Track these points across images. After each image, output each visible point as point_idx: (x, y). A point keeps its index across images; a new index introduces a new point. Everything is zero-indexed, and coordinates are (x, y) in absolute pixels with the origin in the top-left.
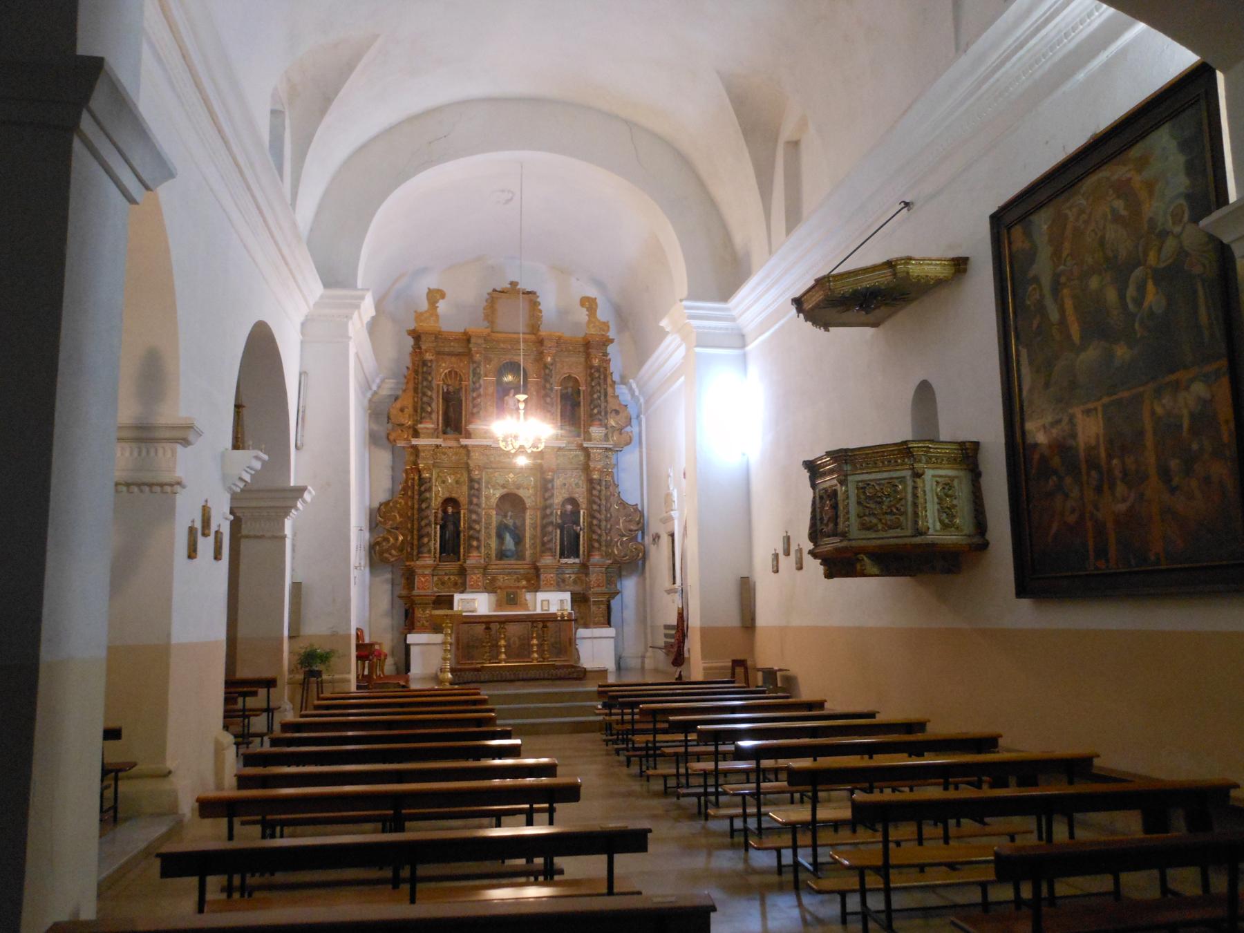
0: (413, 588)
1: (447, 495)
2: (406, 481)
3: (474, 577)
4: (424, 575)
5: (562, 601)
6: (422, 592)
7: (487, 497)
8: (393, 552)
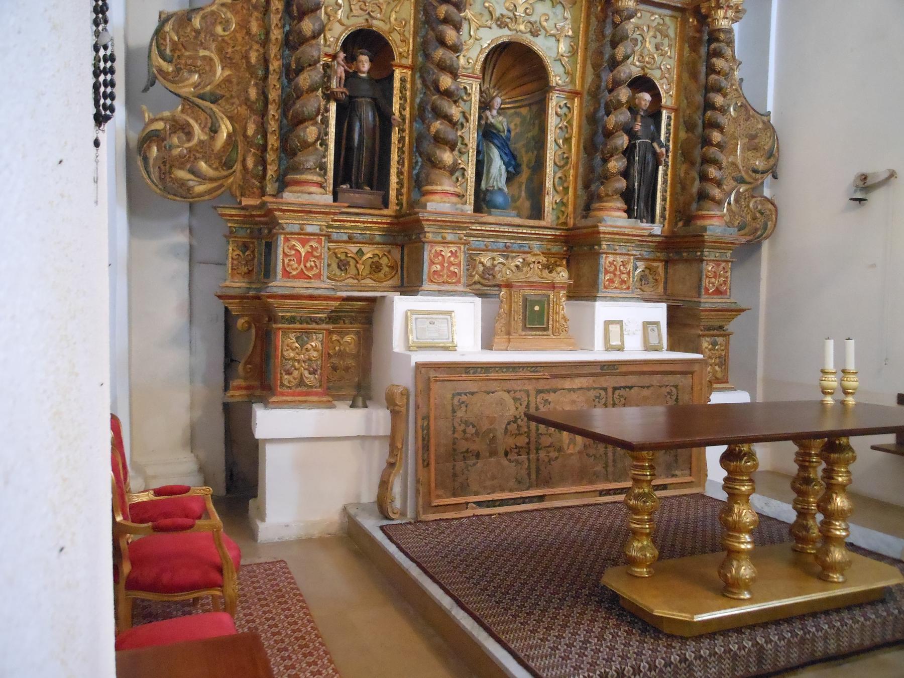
0: (268, 271)
1: (358, 22)
3: (440, 253)
4: (304, 237)
5: (646, 325)
6: (299, 286)
7: (311, 134)
8: (203, 165)
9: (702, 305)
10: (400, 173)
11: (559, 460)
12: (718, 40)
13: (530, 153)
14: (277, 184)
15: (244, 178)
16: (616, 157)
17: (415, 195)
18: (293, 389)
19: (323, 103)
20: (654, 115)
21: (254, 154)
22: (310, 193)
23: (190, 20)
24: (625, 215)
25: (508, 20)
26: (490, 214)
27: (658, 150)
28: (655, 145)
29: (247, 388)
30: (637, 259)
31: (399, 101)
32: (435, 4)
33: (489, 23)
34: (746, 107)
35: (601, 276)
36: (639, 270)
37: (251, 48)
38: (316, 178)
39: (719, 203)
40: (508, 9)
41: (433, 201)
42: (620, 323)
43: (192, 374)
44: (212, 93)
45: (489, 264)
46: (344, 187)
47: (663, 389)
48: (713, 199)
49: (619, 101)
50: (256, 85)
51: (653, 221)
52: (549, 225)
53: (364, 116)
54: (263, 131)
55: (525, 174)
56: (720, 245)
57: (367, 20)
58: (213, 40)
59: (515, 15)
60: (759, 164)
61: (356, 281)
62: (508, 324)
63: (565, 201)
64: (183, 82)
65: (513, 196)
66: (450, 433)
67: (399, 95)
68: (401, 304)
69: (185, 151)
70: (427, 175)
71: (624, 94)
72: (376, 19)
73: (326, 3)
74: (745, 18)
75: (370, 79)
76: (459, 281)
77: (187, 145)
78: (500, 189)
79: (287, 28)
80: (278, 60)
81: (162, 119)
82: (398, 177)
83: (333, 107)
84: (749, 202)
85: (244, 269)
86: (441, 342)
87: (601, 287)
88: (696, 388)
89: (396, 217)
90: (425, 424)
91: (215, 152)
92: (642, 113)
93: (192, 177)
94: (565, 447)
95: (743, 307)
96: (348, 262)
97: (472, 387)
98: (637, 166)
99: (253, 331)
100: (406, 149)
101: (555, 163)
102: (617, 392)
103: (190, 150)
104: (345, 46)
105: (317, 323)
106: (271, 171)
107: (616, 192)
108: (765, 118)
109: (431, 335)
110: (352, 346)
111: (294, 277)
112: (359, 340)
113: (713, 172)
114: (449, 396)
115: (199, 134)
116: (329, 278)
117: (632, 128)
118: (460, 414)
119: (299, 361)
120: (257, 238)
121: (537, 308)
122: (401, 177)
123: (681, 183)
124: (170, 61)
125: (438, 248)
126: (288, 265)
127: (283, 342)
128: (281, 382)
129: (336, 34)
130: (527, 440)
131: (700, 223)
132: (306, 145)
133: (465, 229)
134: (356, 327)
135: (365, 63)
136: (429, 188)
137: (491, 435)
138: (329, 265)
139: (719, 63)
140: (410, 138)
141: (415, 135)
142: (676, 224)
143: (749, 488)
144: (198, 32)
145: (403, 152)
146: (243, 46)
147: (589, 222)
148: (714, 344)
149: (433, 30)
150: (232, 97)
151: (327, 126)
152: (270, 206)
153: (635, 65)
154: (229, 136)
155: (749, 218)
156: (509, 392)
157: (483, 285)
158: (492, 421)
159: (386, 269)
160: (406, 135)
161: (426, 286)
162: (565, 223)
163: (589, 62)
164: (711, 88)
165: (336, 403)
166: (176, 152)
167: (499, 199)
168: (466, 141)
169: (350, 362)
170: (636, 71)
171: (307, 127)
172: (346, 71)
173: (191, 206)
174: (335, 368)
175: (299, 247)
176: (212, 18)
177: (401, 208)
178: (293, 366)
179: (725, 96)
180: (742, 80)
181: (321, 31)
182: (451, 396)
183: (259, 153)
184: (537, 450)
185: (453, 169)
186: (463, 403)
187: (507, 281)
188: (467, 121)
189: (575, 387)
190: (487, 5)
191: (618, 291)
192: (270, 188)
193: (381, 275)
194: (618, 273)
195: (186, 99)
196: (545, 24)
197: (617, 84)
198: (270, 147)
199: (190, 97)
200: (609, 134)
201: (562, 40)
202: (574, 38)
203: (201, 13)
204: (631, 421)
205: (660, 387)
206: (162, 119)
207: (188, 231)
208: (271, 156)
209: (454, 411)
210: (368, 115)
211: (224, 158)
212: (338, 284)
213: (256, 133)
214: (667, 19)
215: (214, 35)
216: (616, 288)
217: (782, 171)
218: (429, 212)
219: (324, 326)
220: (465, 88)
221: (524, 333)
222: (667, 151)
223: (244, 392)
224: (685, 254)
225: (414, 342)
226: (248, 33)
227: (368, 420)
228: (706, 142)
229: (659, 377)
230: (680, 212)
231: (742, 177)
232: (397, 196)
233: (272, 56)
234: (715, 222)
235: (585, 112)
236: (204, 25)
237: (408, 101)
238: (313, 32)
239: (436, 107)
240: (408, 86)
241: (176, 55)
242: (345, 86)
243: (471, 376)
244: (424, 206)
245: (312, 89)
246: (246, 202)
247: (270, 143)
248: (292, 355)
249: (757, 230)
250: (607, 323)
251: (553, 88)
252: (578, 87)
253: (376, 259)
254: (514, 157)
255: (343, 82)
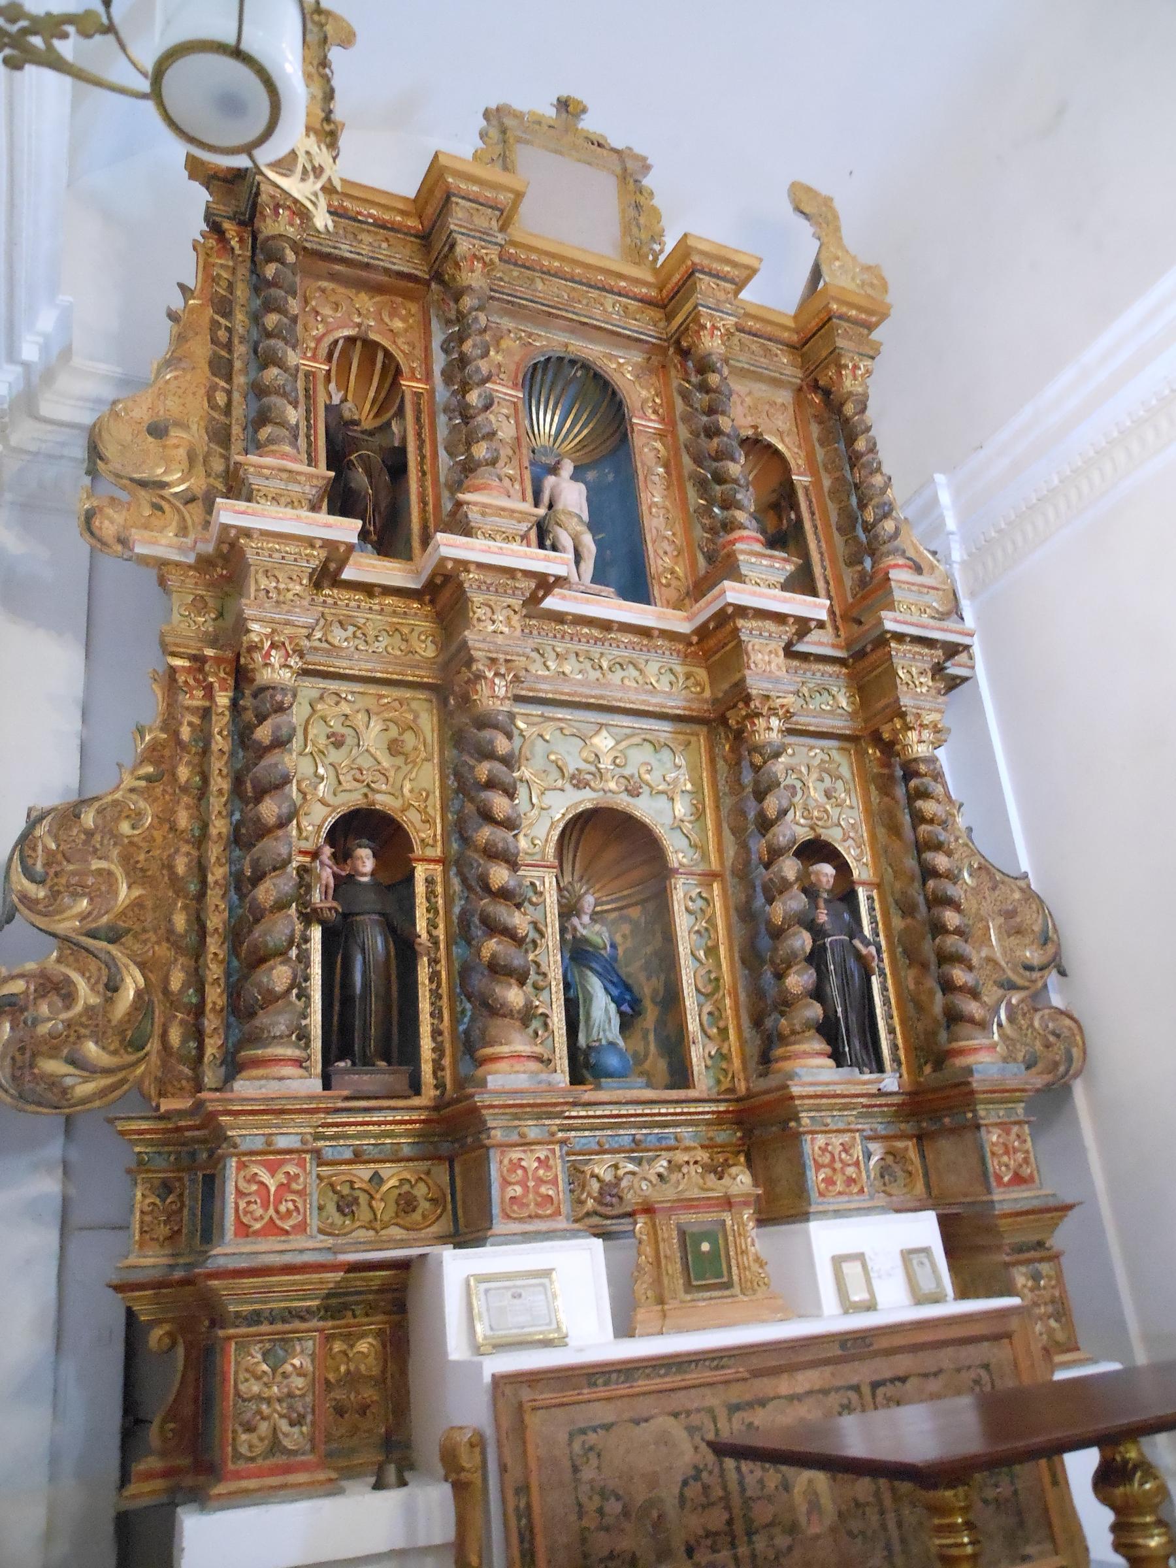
0: (209, 1230)
1: (352, 799)
2: (170, 724)
3: (519, 1164)
4: (273, 1157)
5: (908, 1255)
6: (268, 1251)
8: (91, 1048)
9: (997, 1206)
10: (436, 1033)
11: (797, 1554)
12: (917, 774)
13: (654, 980)
14: (223, 1069)
15: (164, 1064)
16: (794, 969)
17: (465, 1068)
18: (260, 1461)
19: (299, 927)
20: (846, 895)
21: (182, 1022)
22: (281, 1079)
23: (78, 816)
24: (830, 1062)
25: (588, 777)
26: (598, 1087)
27: (864, 951)
28: (857, 943)
29: (166, 1474)
30: (869, 1138)
31: (426, 915)
32: (472, 762)
33: (560, 783)
34: (987, 869)
35: (811, 1174)
36: (875, 1159)
37: (177, 851)
38: (291, 1052)
39: (983, 1025)
40: (586, 761)
41: (496, 1073)
42: (860, 1257)
43: (54, 1457)
44: (111, 927)
45: (608, 1177)
46: (342, 1064)
47: (964, 1374)
48: (972, 1020)
49: (784, 880)
50: (185, 907)
51: (881, 1069)
52: (705, 1096)
53: (369, 943)
54: (198, 982)
55: (651, 1015)
56: (1004, 1095)
57: (366, 795)
58: (115, 844)
59: (599, 769)
60: (1031, 955)
61: (372, 1233)
62: (658, 1281)
63: (725, 1051)
64: (62, 912)
65: (635, 1055)
66: (573, 1517)
67: (426, 904)
68: (456, 1267)
69: (60, 1026)
70: (484, 1032)
71: (790, 868)
72: (379, 792)
73: (299, 776)
74: (951, 739)
75: (376, 885)
76: (558, 1213)
77: (65, 1016)
78: (612, 1044)
79: (237, 816)
80: (221, 866)
81: (21, 976)
82: (434, 1038)
83: (316, 933)
84: (1032, 1019)
85: (163, 1231)
86: (537, 1331)
87: (814, 1195)
88: (1024, 1364)
89: (436, 1108)
90: (522, 1505)
91: (114, 1023)
92: (825, 895)
93: (71, 1070)
94: (803, 1520)
95: (1069, 1200)
96: (356, 1200)
97: (604, 1413)
98: (834, 980)
99: (180, 1351)
100: (444, 990)
101: (698, 990)
102: (880, 1391)
103: (69, 1025)
104: (333, 836)
105: (303, 1319)
106: (212, 1047)
107: (808, 1025)
108: (1022, 884)
109: (516, 1322)
110: (371, 1360)
111: (257, 1233)
112: (384, 1346)
113: (960, 975)
114: (563, 1437)
115: (86, 994)
116: (321, 1231)
117: (813, 920)
118: (587, 1474)
119: (268, 1401)
120: (188, 1170)
121: (705, 1247)
122: (440, 1039)
123: (912, 1000)
124: (42, 882)
125: (515, 1154)
126: (246, 1213)
127: (237, 1363)
128: (235, 1449)
129: (316, 821)
130: (726, 1516)
131: (960, 1062)
132: (271, 998)
133: (559, 1115)
134: (377, 1322)
135: (365, 861)
136: (488, 1051)
137: (655, 1514)
138: (321, 1208)
139: (928, 807)
140: (449, 974)
141: (457, 966)
142: (920, 1068)
143: (1163, 1540)
144: (90, 834)
145: (440, 997)
146: (164, 849)
147: (772, 1081)
148: (1036, 1277)
149: (472, 800)
150: (144, 931)
151: (308, 966)
152: (211, 1107)
153: (797, 824)
154: (139, 994)
155: (1038, 1045)
156: (676, 1415)
157: (605, 1215)
158: (653, 1481)
159: (425, 1205)
160: (442, 968)
161: (500, 1226)
162: (732, 1090)
163: (725, 826)
164: (924, 846)
165: (344, 1483)
166: (43, 1029)
167: (612, 1061)
168: (544, 968)
169: (369, 1393)
170: (803, 834)
171: (272, 968)
172: (335, 875)
173: (69, 1119)
174: (340, 1411)
175: (265, 1177)
176: (118, 810)
177: (443, 1094)
178: (259, 1412)
179: (949, 854)
180: (970, 829)
181: (294, 814)
182: (566, 1436)
183: (190, 1019)
184: (750, 1533)
185: (527, 1016)
186: (591, 1449)
187: (645, 1202)
188: (542, 935)
189: (799, 1390)
190: (553, 757)
191: (845, 1198)
192: (210, 1077)
193: (417, 1216)
194: (838, 1165)
195: (66, 939)
196: (647, 777)
197: (775, 853)
198: (209, 1006)
199: (73, 935)
200: (777, 934)
201: (677, 798)
202: (698, 791)
203: (96, 805)
204: (915, 1431)
205: (958, 1370)
206: (21, 976)
207: (59, 1171)
208: (211, 1022)
209: (576, 1469)
210: (376, 942)
211: (129, 1033)
212: (340, 1241)
213: (185, 986)
214: (834, 753)
215: (116, 837)
216: (840, 1193)
217: (1070, 960)
218: (490, 1092)
219: (315, 1323)
220: (532, 884)
221: (688, 1297)
222: (879, 951)
223: (159, 1484)
224: (947, 1120)
225: (485, 1338)
226: (173, 828)
227: (410, 1511)
228: (938, 928)
229: (950, 1351)
230: (922, 1049)
231: (1009, 981)
232: (435, 1073)
233: (213, 860)
234: (984, 1058)
235: (731, 904)
236: (100, 822)
237: (441, 912)
238: (279, 817)
239: (488, 916)
240: (439, 889)
241: (52, 872)
242: (334, 898)
243: (602, 1392)
244: (483, 1083)
245: (281, 906)
246: (166, 1105)
247: (209, 1000)
248: (256, 1389)
249: (1057, 1070)
250: (838, 1261)
251: (676, 871)
252: (715, 865)
253: (406, 1187)
254: (628, 988)
255: (331, 892)
